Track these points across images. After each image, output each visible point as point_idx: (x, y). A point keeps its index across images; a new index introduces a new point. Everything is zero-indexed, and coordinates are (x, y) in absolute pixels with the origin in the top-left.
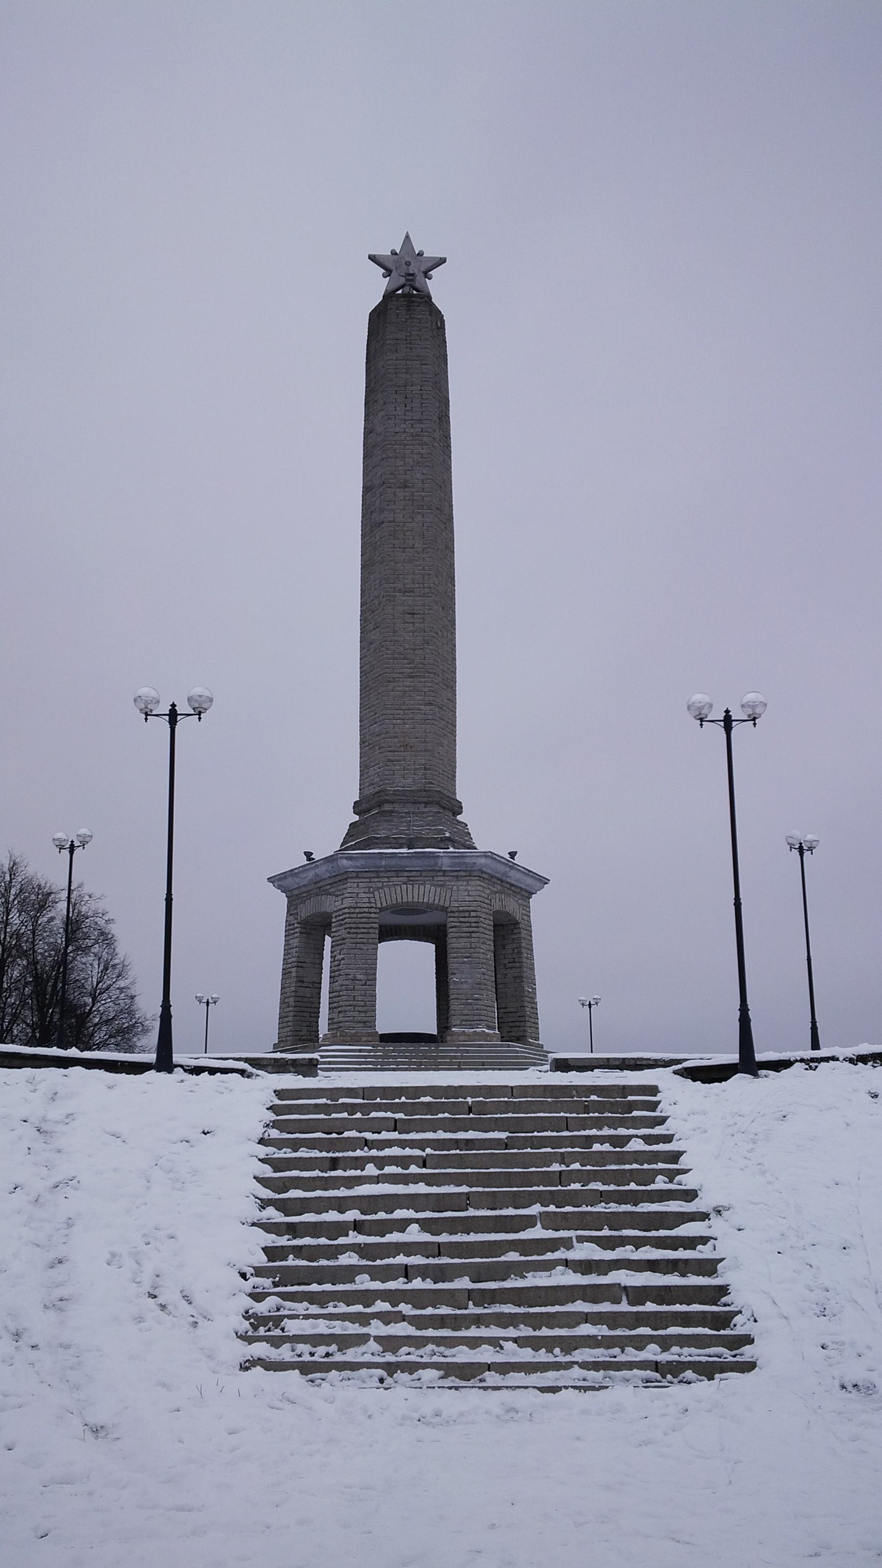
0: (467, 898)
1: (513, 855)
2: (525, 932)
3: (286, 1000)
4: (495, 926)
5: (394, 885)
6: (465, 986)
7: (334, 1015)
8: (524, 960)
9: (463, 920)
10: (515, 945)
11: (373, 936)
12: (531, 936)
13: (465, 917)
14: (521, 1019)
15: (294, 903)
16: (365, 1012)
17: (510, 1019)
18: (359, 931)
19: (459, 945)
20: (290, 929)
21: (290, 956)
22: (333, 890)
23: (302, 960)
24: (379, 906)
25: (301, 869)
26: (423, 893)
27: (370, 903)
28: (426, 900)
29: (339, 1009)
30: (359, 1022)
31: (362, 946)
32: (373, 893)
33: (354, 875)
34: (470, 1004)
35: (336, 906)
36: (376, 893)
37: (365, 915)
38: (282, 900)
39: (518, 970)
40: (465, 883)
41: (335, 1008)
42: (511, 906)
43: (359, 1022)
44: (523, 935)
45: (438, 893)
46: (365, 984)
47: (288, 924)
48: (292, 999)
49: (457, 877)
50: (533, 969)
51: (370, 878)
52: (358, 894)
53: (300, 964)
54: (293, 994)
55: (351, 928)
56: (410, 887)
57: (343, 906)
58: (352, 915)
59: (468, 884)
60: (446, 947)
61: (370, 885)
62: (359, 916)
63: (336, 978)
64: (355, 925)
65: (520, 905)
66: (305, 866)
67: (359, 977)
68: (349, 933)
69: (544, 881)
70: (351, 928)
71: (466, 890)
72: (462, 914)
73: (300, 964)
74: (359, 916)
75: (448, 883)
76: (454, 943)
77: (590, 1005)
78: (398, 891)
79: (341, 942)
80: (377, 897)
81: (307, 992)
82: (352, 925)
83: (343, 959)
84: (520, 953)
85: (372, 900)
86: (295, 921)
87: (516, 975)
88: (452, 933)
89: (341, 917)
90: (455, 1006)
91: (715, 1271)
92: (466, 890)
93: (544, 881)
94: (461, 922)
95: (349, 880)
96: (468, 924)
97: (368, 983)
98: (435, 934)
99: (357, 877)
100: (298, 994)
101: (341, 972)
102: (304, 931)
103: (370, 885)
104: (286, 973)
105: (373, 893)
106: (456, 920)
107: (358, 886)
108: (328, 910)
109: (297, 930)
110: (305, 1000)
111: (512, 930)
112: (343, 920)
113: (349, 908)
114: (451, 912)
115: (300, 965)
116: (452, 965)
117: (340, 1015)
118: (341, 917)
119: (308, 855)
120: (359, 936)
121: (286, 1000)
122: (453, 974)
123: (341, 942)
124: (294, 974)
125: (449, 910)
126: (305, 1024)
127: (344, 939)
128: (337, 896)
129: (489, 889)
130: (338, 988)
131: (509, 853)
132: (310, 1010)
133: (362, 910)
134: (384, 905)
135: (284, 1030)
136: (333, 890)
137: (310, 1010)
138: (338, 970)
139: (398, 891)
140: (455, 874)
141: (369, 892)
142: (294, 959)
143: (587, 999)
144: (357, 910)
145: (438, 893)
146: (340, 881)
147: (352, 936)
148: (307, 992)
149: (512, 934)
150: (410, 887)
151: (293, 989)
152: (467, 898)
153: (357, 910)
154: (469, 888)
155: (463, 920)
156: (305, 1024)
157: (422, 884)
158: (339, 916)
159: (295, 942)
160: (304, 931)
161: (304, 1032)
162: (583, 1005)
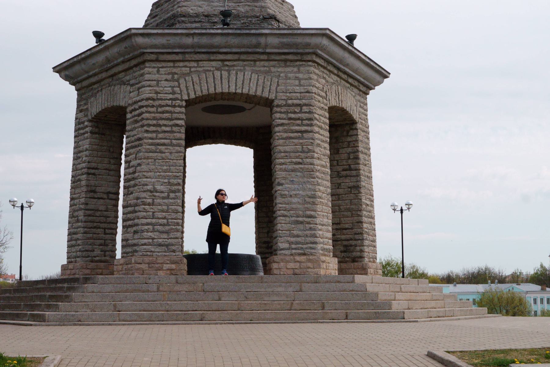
0: (297, 89)
1: (351, 38)
2: (363, 134)
3: (76, 214)
4: (330, 126)
5: (205, 71)
6: (295, 200)
7: (129, 236)
8: (361, 167)
9: (293, 116)
10: (350, 150)
11: (178, 135)
12: (368, 139)
13: (295, 113)
14: (357, 237)
15: (84, 96)
16: (167, 232)
17: (343, 237)
18: (159, 129)
19: (287, 148)
20: (79, 129)
21: (79, 160)
22: (128, 78)
23: (94, 165)
24: (186, 97)
25: (89, 53)
26: (244, 81)
27: (174, 93)
28: (245, 91)
29: (135, 228)
30: (160, 245)
31: (162, 148)
32: (178, 81)
33: (153, 57)
34: (302, 223)
35: (131, 98)
36: (182, 81)
37: (167, 108)
38: (68, 93)
39: (354, 179)
40: (295, 69)
41: (131, 226)
42: (348, 101)
43: (160, 245)
44: (360, 137)
45: (261, 81)
46: (168, 197)
47: (78, 122)
48: (81, 213)
49: (286, 61)
50: (370, 178)
51: (174, 61)
52: (158, 81)
53: (92, 171)
54: (82, 207)
55: (149, 125)
56: (225, 74)
57: (138, 98)
58: (150, 109)
59: (299, 72)
60: (270, 156)
61: (174, 70)
62: (160, 110)
63: (131, 189)
64: (155, 122)
65: (356, 100)
66: (94, 47)
67: (159, 187)
68: (147, 131)
69: (384, 75)
70: (149, 125)
71: (297, 78)
72: (292, 109)
73: (92, 171)
74: (160, 110)
75: (273, 69)
76: (281, 145)
77: (402, 211)
78: (211, 80)
79: (137, 143)
80: (183, 86)
81: (100, 205)
82: (151, 122)
83: (139, 165)
84: (357, 158)
85: (177, 90)
86: (86, 119)
87: (351, 184)
88: (279, 132)
89: (137, 112)
90: (282, 225)
91: (428, 352)
92: (297, 78)
93: (384, 75)
94: (290, 119)
95: (147, 64)
96: (299, 122)
97: (172, 195)
98: (259, 141)
99: (157, 60)
100: (89, 207)
101: (137, 181)
102: (97, 130)
103: (174, 70)
104: (75, 181)
105: (178, 81)
106: (284, 116)
107: (158, 72)
108: (122, 104)
109: (88, 129)
110: (98, 214)
111: (348, 132)
112: (139, 115)
113: (148, 99)
114: (278, 106)
115: (91, 171)
116: (279, 174)
117: (136, 236)
118: (137, 112)
119: (98, 35)
120: (160, 135)
121: (76, 214)
122: (280, 184)
123: (137, 143)
124: (83, 183)
125: (275, 103)
126: (99, 242)
127: (140, 139)
128: (132, 85)
129: (324, 78)
130: (133, 202)
131: (348, 37)
132: (105, 225)
133: (163, 103)
134: (192, 96)
135: (74, 249)
136: (128, 78)
137: (105, 225)
138: (134, 179)
139: (211, 80)
140: (283, 57)
141: (173, 80)
142: (84, 165)
143: (400, 204)
144: (157, 103)
145: (261, 81)
146: (136, 66)
147: (150, 135)
148: (100, 205)
149: (347, 136)
150: (225, 74)
151: (83, 200)
152: (297, 89)
153: (157, 103)
154: (301, 76)
155: (293, 116)
156: (99, 242)
157: (241, 70)
158: (135, 110)
159: (86, 144)
160: (97, 130)
161: (97, 252)
162: (394, 210)
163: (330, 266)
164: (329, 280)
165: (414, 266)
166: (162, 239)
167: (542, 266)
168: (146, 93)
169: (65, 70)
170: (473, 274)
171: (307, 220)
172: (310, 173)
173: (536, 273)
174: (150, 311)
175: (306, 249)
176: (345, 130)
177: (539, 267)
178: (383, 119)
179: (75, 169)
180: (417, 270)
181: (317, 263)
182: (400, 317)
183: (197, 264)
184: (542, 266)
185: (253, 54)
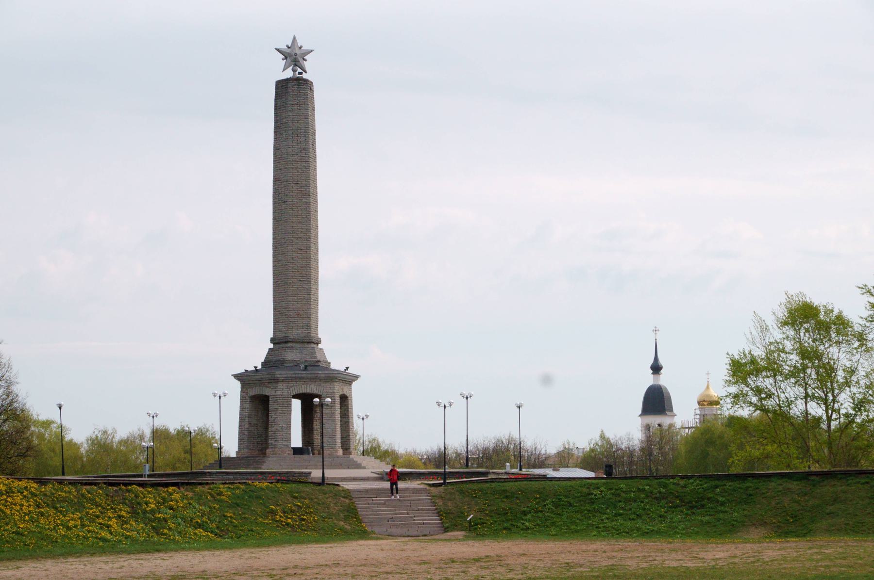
38: (238, 384)
42: (345, 391)
163: (340, 452)
164: (338, 457)
165: (374, 440)
166: (285, 443)
167: (602, 437)
168: (279, 393)
169: (237, 377)
170: (485, 451)
171: (333, 436)
172: (334, 421)
173: (592, 450)
174: (236, 473)
175: (333, 447)
176: (345, 400)
177: (598, 438)
178: (358, 394)
179: (241, 414)
180: (379, 446)
181: (337, 451)
182: (364, 468)
183: (296, 451)
184: (602, 437)
185: (315, 379)
